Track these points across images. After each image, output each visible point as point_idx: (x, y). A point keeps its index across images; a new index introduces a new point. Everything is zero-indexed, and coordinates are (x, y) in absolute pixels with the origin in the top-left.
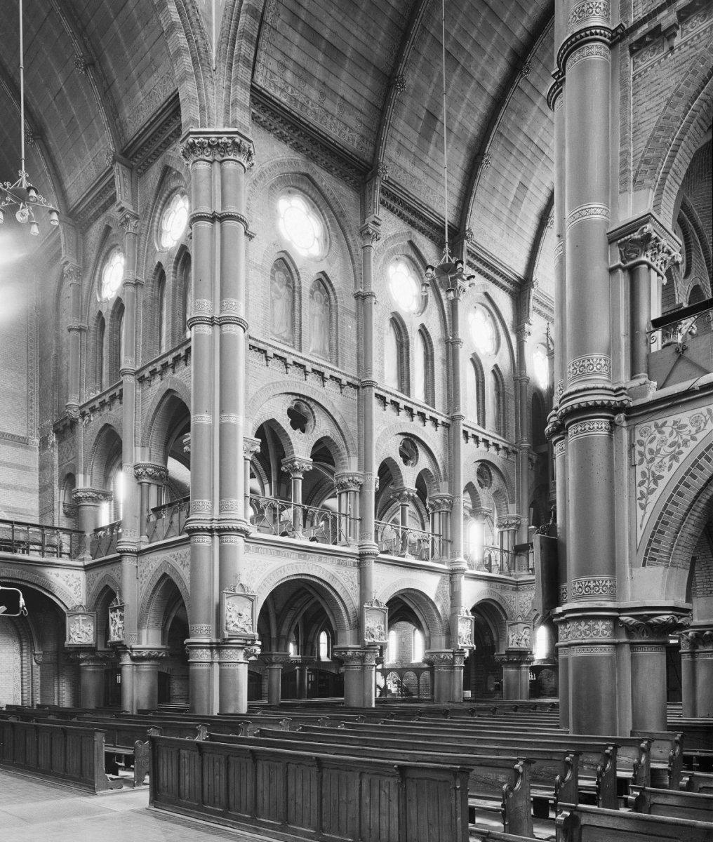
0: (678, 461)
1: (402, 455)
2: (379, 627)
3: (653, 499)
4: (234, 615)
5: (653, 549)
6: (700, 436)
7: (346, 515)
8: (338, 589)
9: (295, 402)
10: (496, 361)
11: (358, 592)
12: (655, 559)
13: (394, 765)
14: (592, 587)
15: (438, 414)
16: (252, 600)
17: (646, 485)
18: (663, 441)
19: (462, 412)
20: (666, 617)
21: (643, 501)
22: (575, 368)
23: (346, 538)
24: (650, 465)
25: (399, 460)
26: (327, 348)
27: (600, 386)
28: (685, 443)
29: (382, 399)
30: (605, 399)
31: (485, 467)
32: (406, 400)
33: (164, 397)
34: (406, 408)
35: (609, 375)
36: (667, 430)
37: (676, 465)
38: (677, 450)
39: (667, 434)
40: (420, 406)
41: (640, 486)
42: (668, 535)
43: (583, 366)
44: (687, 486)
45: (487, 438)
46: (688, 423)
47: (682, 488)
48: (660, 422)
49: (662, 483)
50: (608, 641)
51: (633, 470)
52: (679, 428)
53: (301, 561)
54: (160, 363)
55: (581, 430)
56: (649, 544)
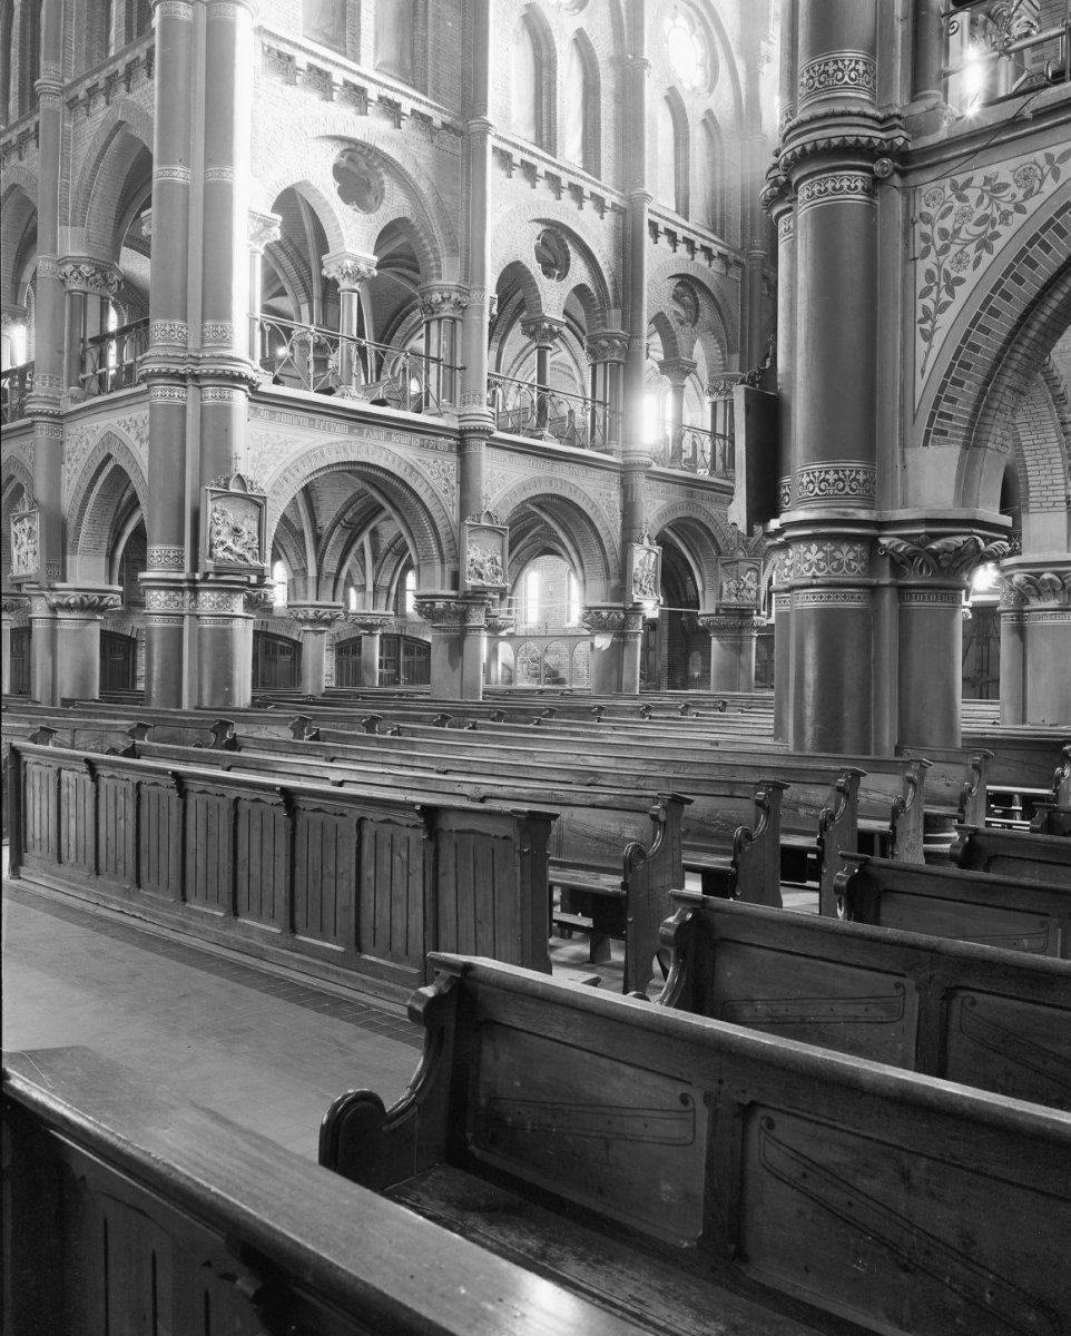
0: (990, 251)
1: (540, 258)
2: (493, 561)
3: (945, 320)
4: (225, 530)
5: (942, 415)
6: (1031, 205)
7: (438, 360)
8: (420, 491)
9: (347, 154)
10: (710, 103)
11: (456, 499)
12: (944, 433)
13: (414, 804)
14: (831, 481)
15: (605, 189)
16: (260, 506)
17: (933, 295)
18: (964, 215)
19: (647, 189)
20: (960, 539)
21: (927, 326)
22: (811, 77)
23: (438, 404)
24: (941, 258)
25: (535, 268)
26: (408, 61)
27: (855, 109)
28: (1005, 216)
29: (505, 159)
30: (864, 133)
31: (687, 285)
32: (592, 182)
33: (111, 136)
34: (548, 175)
35: (872, 92)
36: (972, 194)
37: (987, 258)
38: (990, 231)
39: (973, 202)
40: (573, 174)
41: (922, 296)
42: (970, 387)
43: (825, 72)
44: (1007, 296)
45: (692, 236)
46: (1011, 182)
47: (997, 300)
48: (960, 179)
49: (962, 292)
50: (856, 580)
51: (911, 265)
52: (994, 190)
53: (351, 438)
54: (105, 73)
55: (820, 192)
56: (936, 405)
